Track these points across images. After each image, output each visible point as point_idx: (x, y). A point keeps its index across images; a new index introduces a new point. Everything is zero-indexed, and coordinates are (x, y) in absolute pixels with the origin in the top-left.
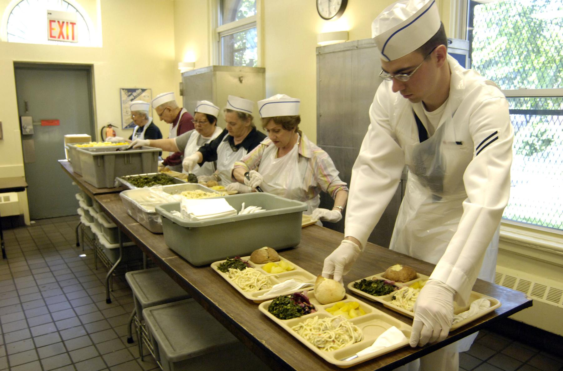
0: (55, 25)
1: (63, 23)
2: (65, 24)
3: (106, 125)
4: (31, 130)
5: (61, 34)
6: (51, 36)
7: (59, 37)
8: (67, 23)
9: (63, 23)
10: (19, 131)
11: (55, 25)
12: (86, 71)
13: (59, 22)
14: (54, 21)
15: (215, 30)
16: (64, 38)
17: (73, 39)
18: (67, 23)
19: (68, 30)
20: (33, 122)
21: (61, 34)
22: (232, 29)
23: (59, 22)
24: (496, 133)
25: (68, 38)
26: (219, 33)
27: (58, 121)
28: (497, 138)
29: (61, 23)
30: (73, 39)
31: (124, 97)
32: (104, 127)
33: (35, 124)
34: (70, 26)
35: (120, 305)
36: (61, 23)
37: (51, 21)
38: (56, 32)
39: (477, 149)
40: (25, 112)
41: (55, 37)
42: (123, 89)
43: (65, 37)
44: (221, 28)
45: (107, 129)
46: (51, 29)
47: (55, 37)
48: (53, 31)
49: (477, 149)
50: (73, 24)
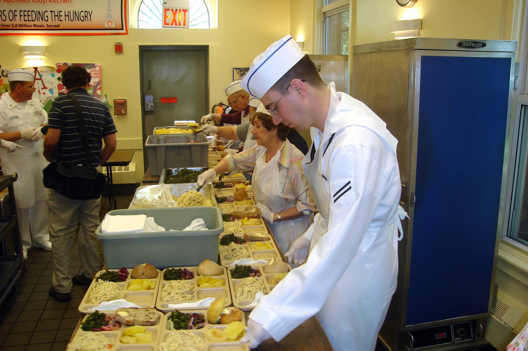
0: (170, 15)
1: (177, 10)
2: (178, 11)
3: (217, 104)
4: (152, 106)
5: (174, 21)
6: (165, 24)
7: (172, 24)
8: (180, 10)
9: (177, 10)
10: (140, 107)
11: (170, 15)
12: (201, 52)
13: (172, 10)
14: (169, 10)
15: (321, 10)
16: (176, 25)
17: (184, 25)
18: (180, 10)
19: (180, 17)
20: (154, 99)
21: (174, 21)
22: (334, 9)
23: (172, 10)
24: (349, 182)
25: (180, 25)
26: (324, 13)
27: (175, 98)
28: (350, 188)
29: (174, 10)
30: (184, 25)
31: (237, 76)
32: (216, 105)
33: (155, 101)
34: (182, 13)
35: (36, 284)
36: (174, 10)
37: (166, 10)
38: (169, 21)
39: (334, 196)
40: (149, 90)
41: (168, 24)
42: (236, 69)
43: (178, 24)
44: (326, 9)
45: (218, 108)
46: (165, 17)
47: (168, 24)
48: (167, 19)
49: (334, 196)
50: (185, 11)
